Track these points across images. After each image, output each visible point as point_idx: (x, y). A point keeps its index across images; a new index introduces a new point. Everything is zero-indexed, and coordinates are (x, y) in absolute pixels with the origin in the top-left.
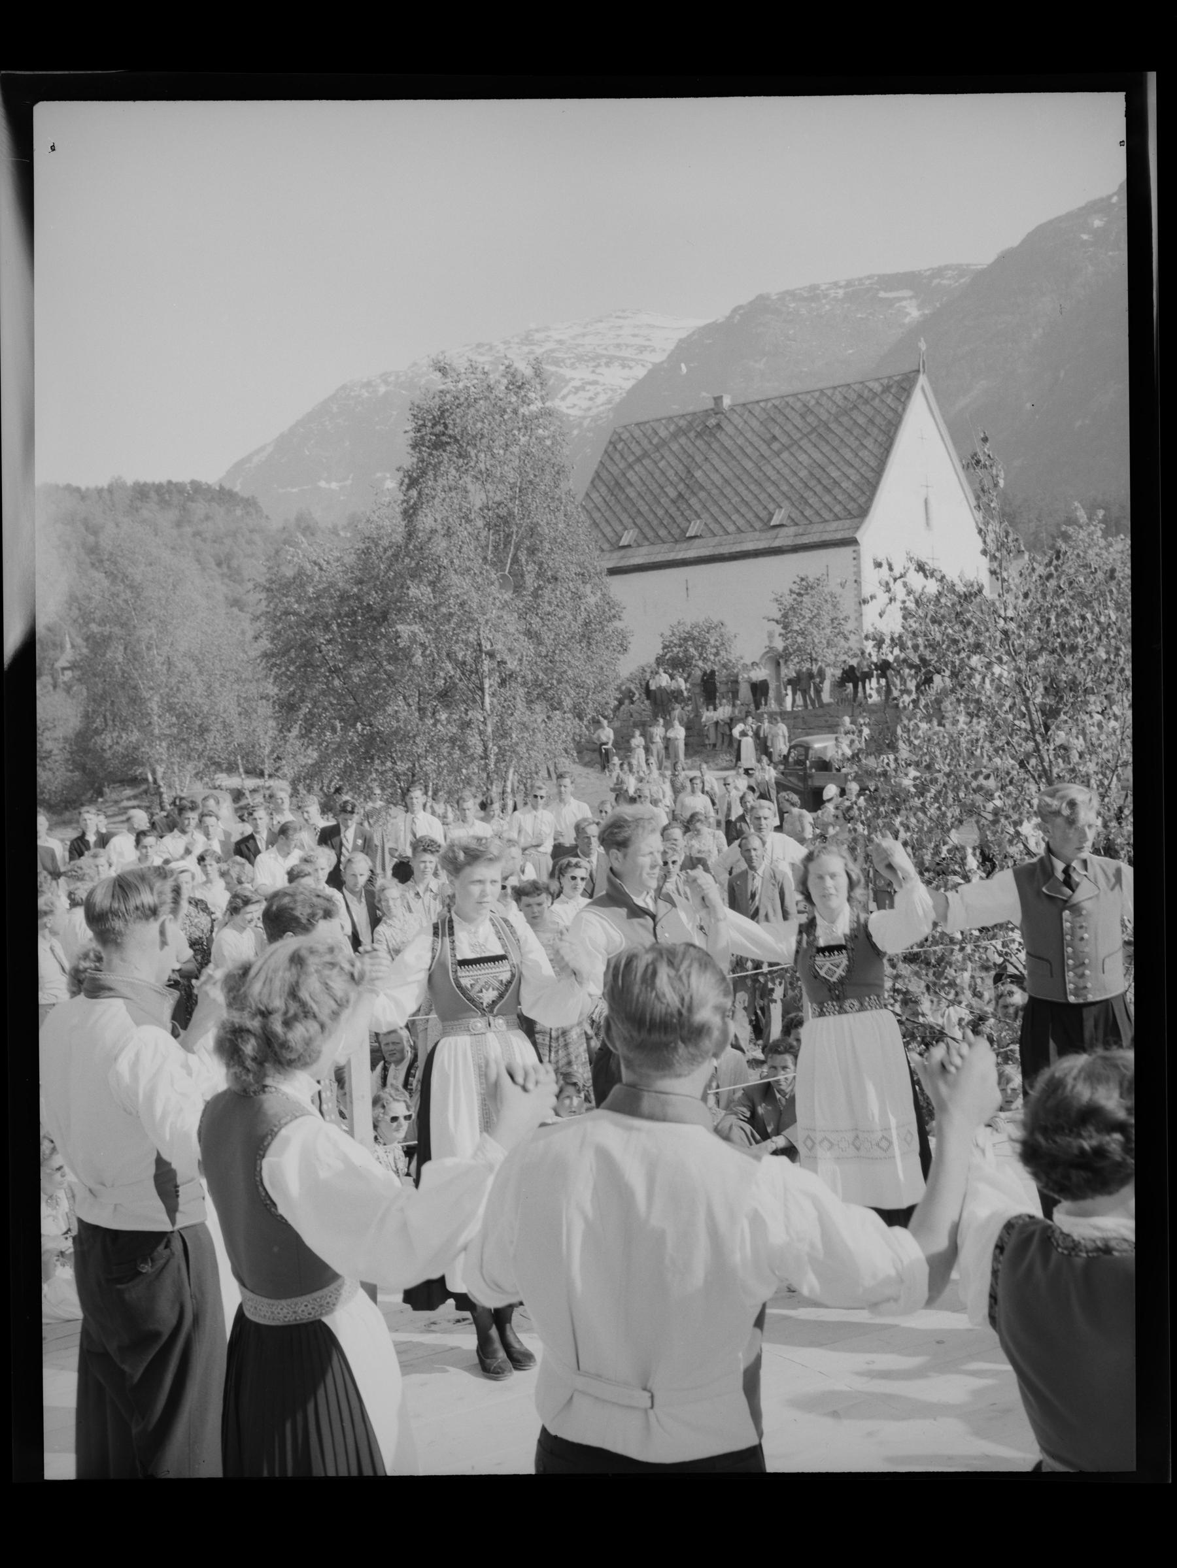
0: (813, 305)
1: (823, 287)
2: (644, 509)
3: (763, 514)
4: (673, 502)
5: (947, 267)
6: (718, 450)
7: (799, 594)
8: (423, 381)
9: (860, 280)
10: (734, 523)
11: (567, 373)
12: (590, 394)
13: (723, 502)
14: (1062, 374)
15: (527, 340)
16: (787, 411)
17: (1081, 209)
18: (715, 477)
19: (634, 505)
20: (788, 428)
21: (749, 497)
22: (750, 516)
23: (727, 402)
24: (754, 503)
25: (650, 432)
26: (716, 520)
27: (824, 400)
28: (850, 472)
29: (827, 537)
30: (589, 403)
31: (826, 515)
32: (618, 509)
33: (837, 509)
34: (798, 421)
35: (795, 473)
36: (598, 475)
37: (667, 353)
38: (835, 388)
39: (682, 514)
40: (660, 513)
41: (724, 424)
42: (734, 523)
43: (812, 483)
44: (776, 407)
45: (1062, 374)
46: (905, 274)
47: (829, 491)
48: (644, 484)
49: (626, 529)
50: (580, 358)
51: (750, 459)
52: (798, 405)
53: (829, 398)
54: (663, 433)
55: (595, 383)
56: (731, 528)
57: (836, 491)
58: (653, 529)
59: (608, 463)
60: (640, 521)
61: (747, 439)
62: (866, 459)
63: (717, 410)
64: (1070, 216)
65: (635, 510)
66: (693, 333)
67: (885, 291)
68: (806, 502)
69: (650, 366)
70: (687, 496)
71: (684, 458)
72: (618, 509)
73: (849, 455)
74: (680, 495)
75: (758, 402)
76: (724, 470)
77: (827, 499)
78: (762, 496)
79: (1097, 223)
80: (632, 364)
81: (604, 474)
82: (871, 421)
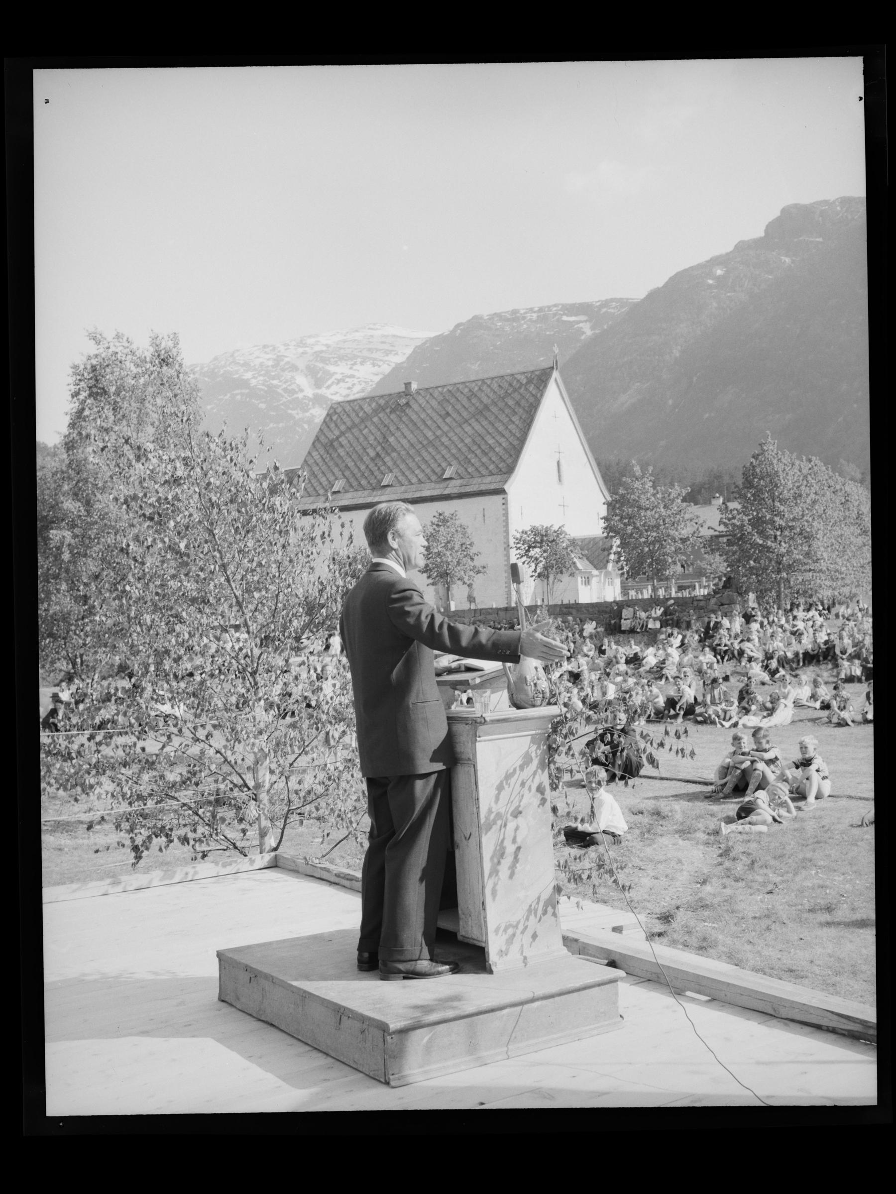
0: (515, 324)
1: (522, 312)
2: (351, 464)
3: (438, 470)
4: (372, 459)
5: (612, 300)
6: (407, 422)
7: (438, 525)
8: (222, 372)
9: (549, 307)
10: (417, 476)
11: (331, 368)
12: (349, 385)
13: (409, 461)
14: (695, 379)
15: (301, 343)
16: (458, 394)
17: (708, 262)
18: (404, 442)
19: (344, 461)
20: (458, 407)
21: (428, 458)
22: (428, 471)
23: (414, 386)
24: (431, 462)
25: (357, 407)
26: (403, 474)
27: (485, 388)
28: (502, 440)
29: (483, 487)
30: (347, 392)
31: (484, 472)
32: (331, 464)
33: (492, 467)
34: (465, 402)
35: (462, 441)
36: (318, 438)
37: (407, 355)
38: (493, 379)
39: (379, 469)
40: (363, 467)
41: (412, 403)
42: (417, 476)
43: (474, 448)
44: (450, 391)
45: (695, 379)
46: (581, 304)
47: (486, 454)
48: (351, 446)
49: (337, 479)
50: (342, 358)
51: (430, 429)
52: (466, 390)
53: (489, 386)
54: (367, 408)
55: (352, 376)
56: (414, 480)
57: (491, 454)
58: (357, 479)
59: (326, 430)
60: (347, 473)
61: (428, 415)
62: (514, 431)
63: (407, 393)
64: (700, 266)
65: (344, 465)
66: (425, 343)
67: (567, 316)
68: (470, 462)
69: (393, 365)
70: (383, 456)
71: (381, 427)
72: (331, 464)
73: (501, 428)
74: (378, 455)
75: (437, 387)
76: (410, 436)
77: (484, 460)
78: (438, 457)
79: (719, 272)
80: (380, 363)
81: (322, 438)
82: (518, 404)
